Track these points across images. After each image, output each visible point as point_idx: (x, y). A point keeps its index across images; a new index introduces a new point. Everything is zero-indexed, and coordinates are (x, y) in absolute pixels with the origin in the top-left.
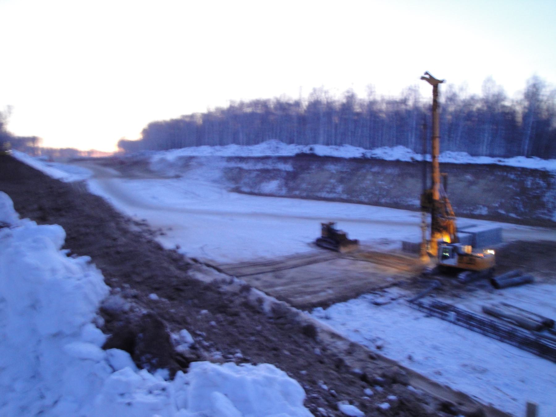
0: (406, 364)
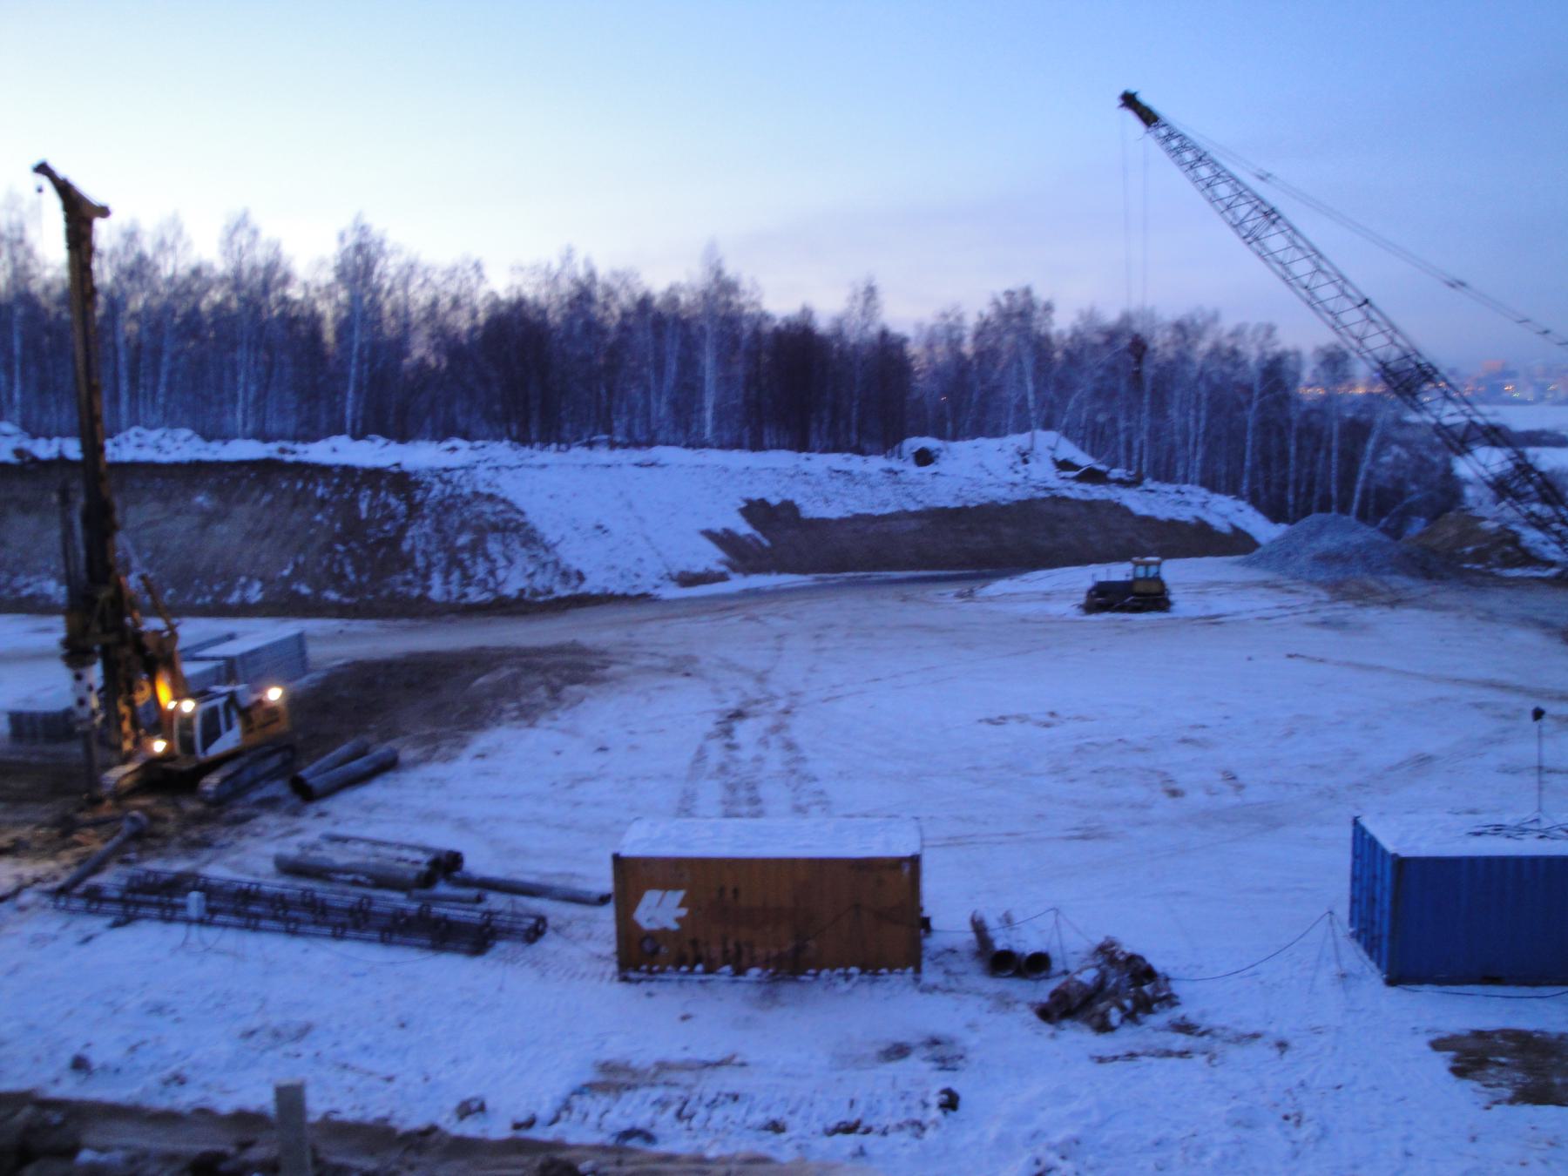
0: (69, 1088)
